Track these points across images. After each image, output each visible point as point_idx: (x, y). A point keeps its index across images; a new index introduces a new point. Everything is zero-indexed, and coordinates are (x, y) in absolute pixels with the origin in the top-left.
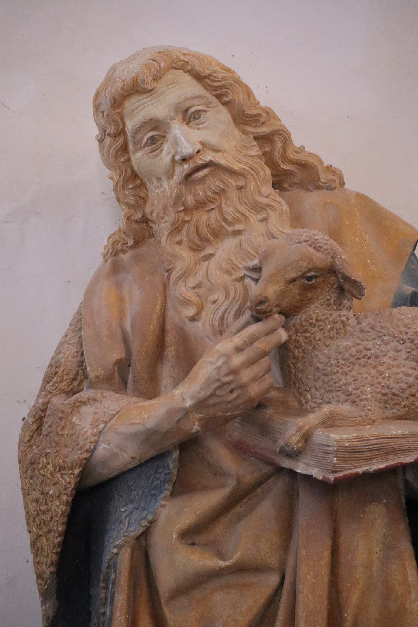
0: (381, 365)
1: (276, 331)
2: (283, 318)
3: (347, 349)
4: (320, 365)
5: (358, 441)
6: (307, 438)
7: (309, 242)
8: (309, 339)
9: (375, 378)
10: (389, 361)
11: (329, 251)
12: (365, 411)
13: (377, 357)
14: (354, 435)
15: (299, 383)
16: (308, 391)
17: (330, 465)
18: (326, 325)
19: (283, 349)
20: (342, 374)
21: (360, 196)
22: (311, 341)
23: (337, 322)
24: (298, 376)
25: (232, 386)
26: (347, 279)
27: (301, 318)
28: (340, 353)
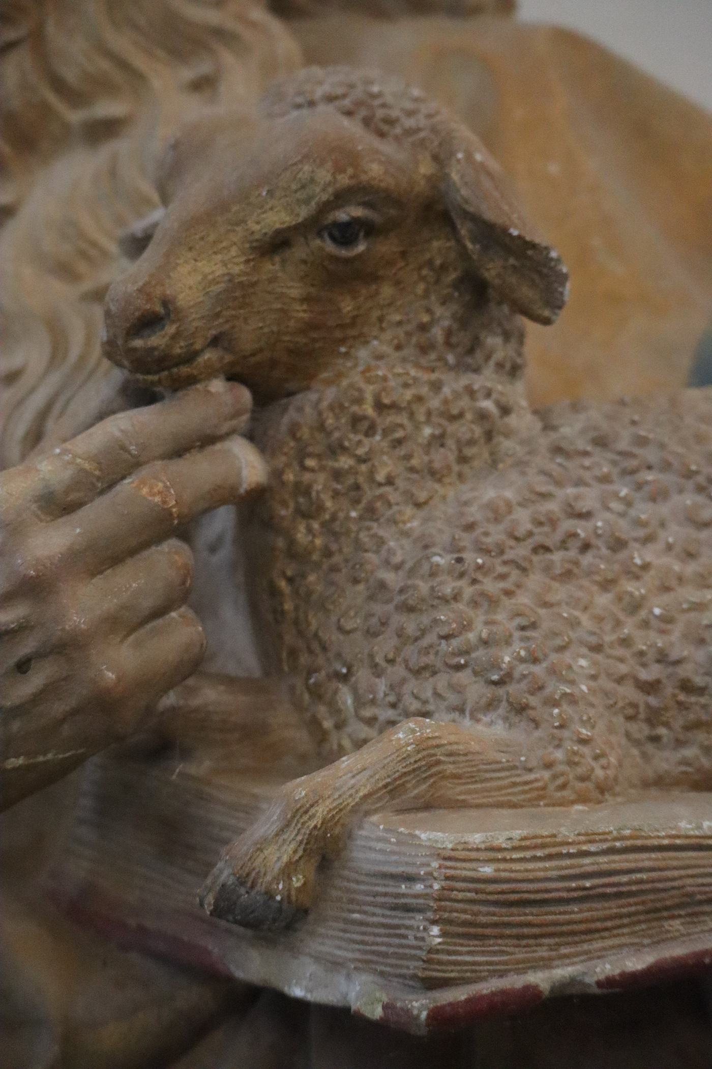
0: (636, 573)
1: (218, 446)
2: (246, 395)
3: (496, 513)
4: (389, 577)
5: (535, 859)
6: (326, 851)
7: (347, 102)
8: (350, 481)
9: (608, 627)
10: (665, 560)
11: (422, 135)
12: (569, 745)
13: (618, 545)
14: (517, 834)
15: (311, 651)
16: (345, 678)
17: (414, 958)
18: (417, 427)
19: (254, 507)
20: (474, 603)
21: (570, 42)
22: (357, 487)
23: (461, 415)
24: (309, 624)
25: (27, 646)
26: (493, 236)
27: (320, 400)
28: (470, 527)
